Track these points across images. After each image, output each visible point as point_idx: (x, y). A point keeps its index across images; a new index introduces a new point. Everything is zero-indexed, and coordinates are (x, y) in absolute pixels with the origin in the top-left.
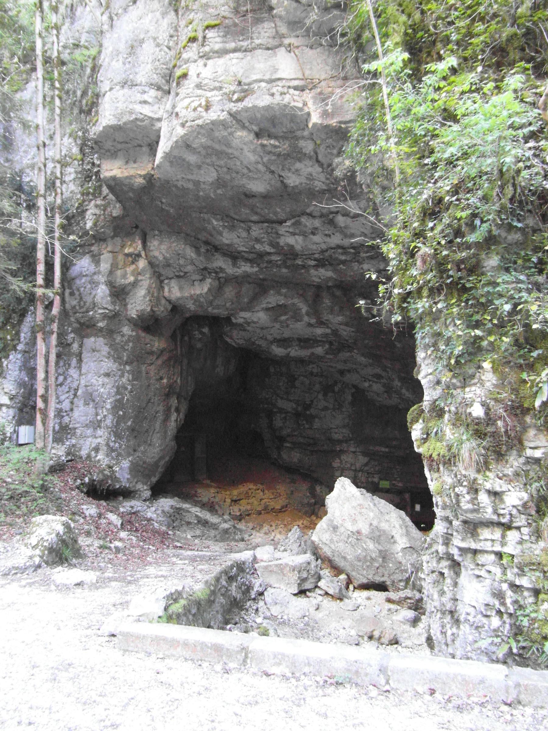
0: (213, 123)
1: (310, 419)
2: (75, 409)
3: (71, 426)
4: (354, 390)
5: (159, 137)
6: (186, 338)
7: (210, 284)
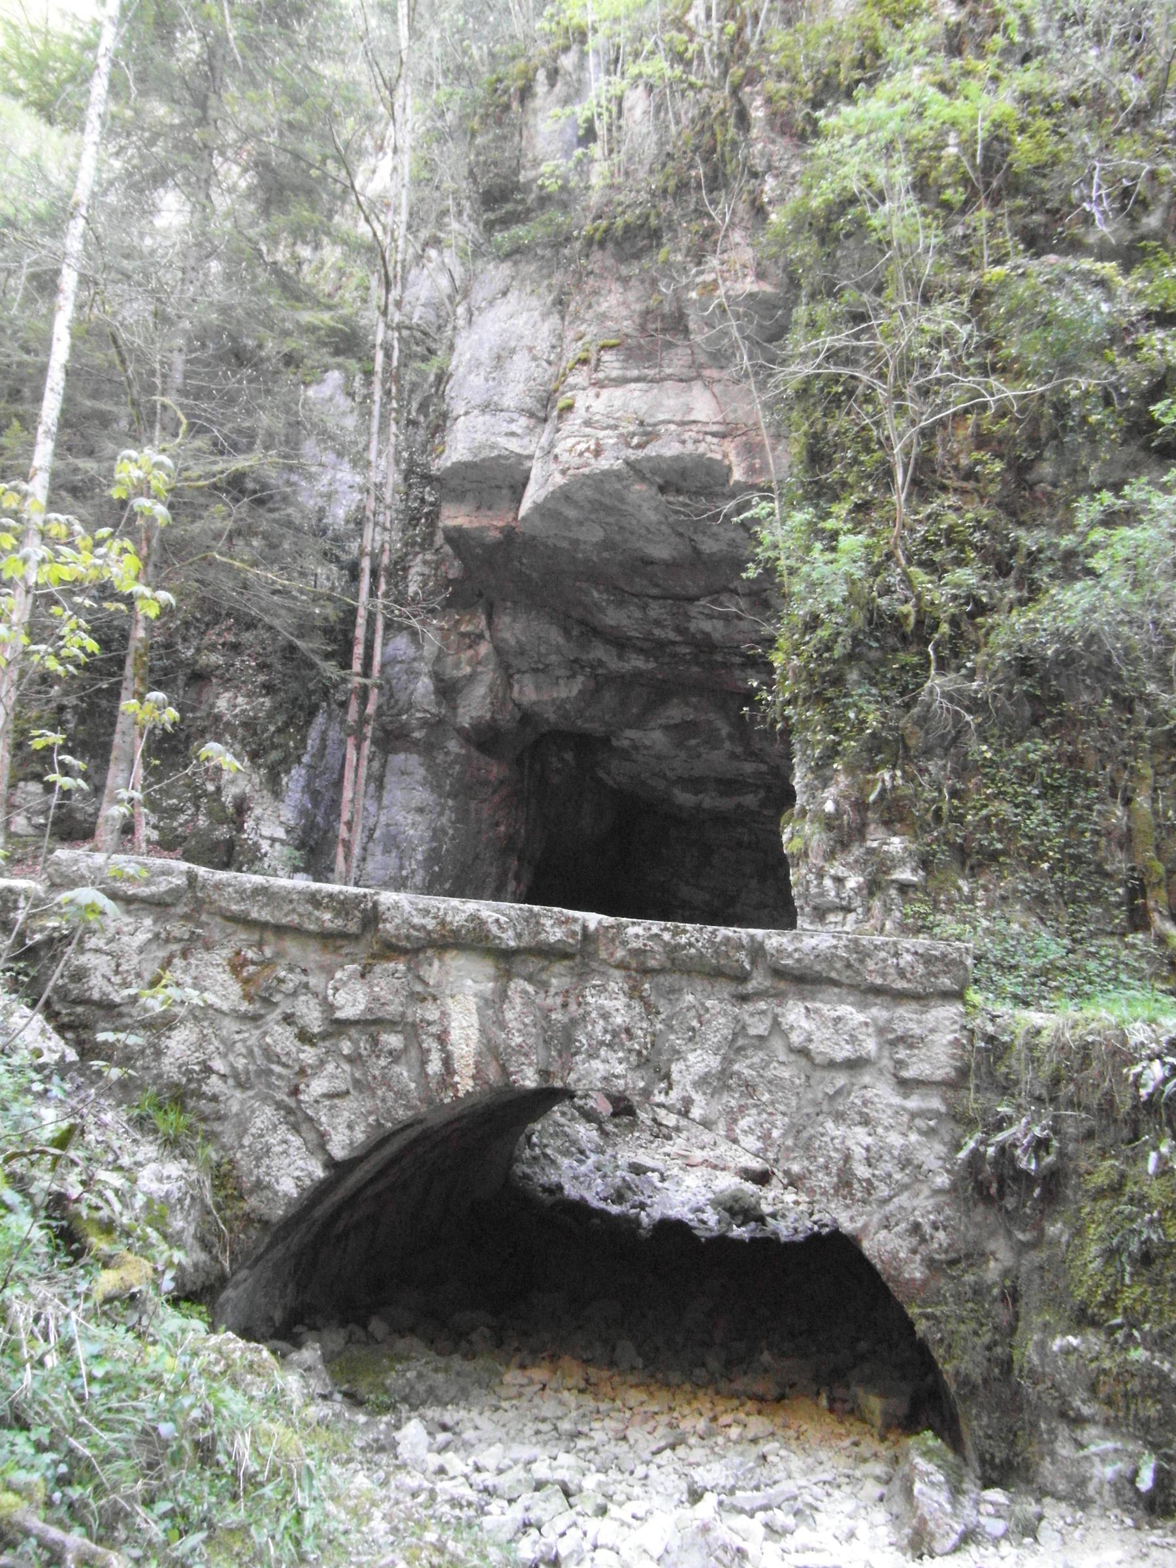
0: (604, 473)
5: (528, 478)
6: (538, 767)
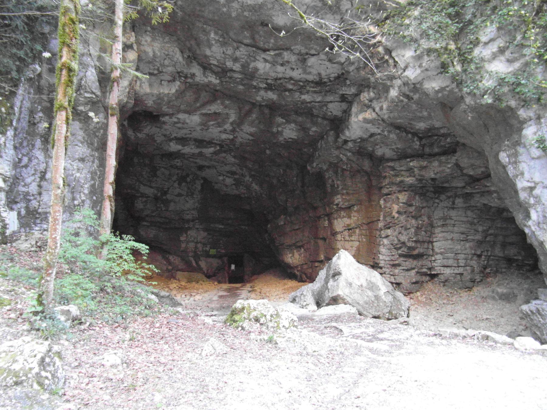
1: (167, 202)
2: (44, 193)
3: (40, 210)
4: (202, 181)
7: (179, 86)
